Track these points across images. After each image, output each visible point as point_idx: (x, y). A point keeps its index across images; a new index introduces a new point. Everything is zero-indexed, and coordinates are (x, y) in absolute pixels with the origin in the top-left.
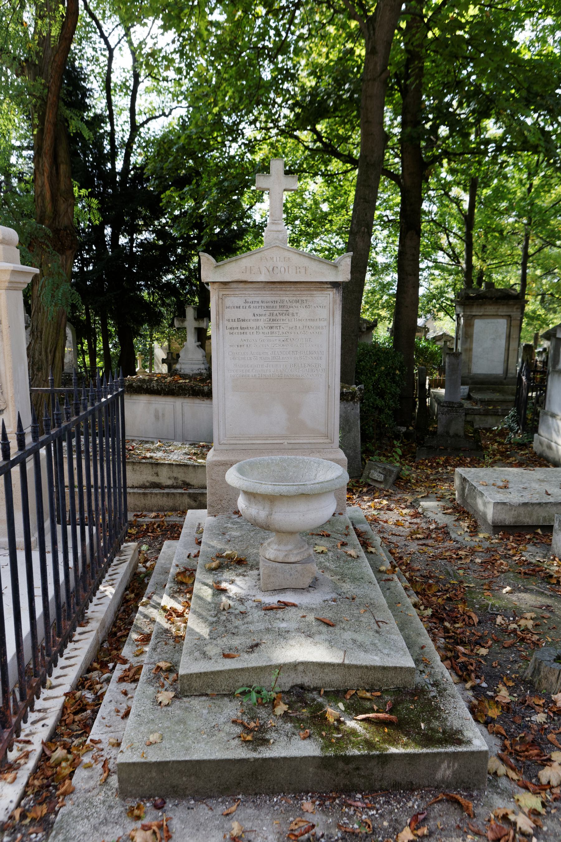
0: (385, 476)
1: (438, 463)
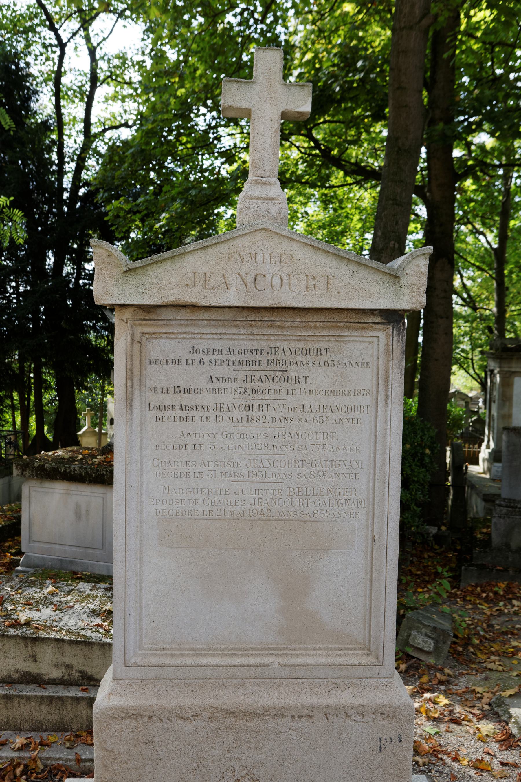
0: (436, 642)
1: (496, 593)
